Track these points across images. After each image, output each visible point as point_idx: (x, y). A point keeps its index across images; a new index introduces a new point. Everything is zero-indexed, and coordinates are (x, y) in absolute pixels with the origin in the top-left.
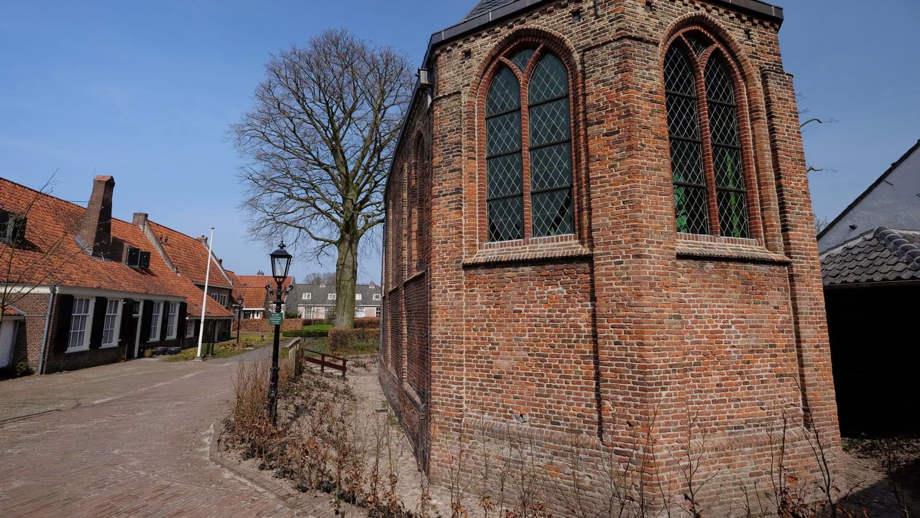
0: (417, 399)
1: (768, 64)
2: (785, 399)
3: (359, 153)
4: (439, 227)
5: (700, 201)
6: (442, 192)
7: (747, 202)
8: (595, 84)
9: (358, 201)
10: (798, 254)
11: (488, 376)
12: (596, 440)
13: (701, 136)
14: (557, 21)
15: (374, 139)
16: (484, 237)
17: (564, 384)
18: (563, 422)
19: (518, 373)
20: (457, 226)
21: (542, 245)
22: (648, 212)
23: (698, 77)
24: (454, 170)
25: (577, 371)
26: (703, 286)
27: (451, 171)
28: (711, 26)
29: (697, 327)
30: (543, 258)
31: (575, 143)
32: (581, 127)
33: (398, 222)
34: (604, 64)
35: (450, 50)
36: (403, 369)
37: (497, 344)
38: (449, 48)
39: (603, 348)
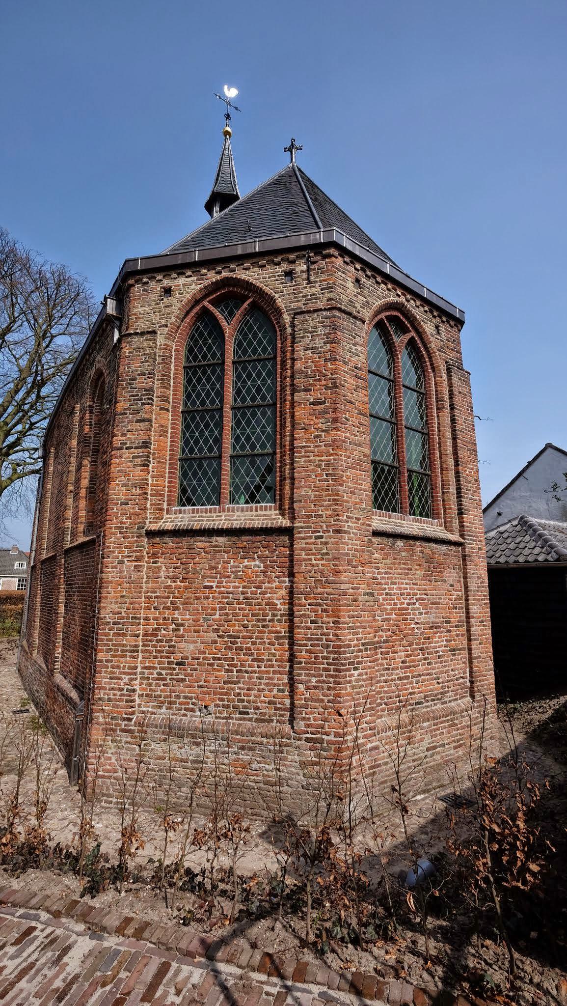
0: (74, 695)
1: (452, 360)
2: (456, 672)
3: (11, 385)
4: (118, 485)
5: (393, 480)
6: (126, 443)
7: (432, 485)
8: (305, 350)
9: (5, 444)
10: (469, 535)
11: (169, 663)
12: (287, 728)
13: (396, 418)
14: (269, 278)
15: (34, 370)
16: (172, 500)
17: (256, 668)
18: (252, 711)
19: (204, 659)
20: (143, 485)
21: (239, 513)
22: (349, 487)
23: (396, 361)
24: (143, 421)
25: (271, 653)
26: (394, 564)
27: (137, 421)
28: (409, 315)
29: (387, 604)
30: (240, 528)
31: (281, 407)
32: (288, 392)
33: (61, 476)
34: (314, 332)
35: (147, 283)
36: (55, 657)
37: (182, 625)
38: (145, 280)
39: (299, 627)
